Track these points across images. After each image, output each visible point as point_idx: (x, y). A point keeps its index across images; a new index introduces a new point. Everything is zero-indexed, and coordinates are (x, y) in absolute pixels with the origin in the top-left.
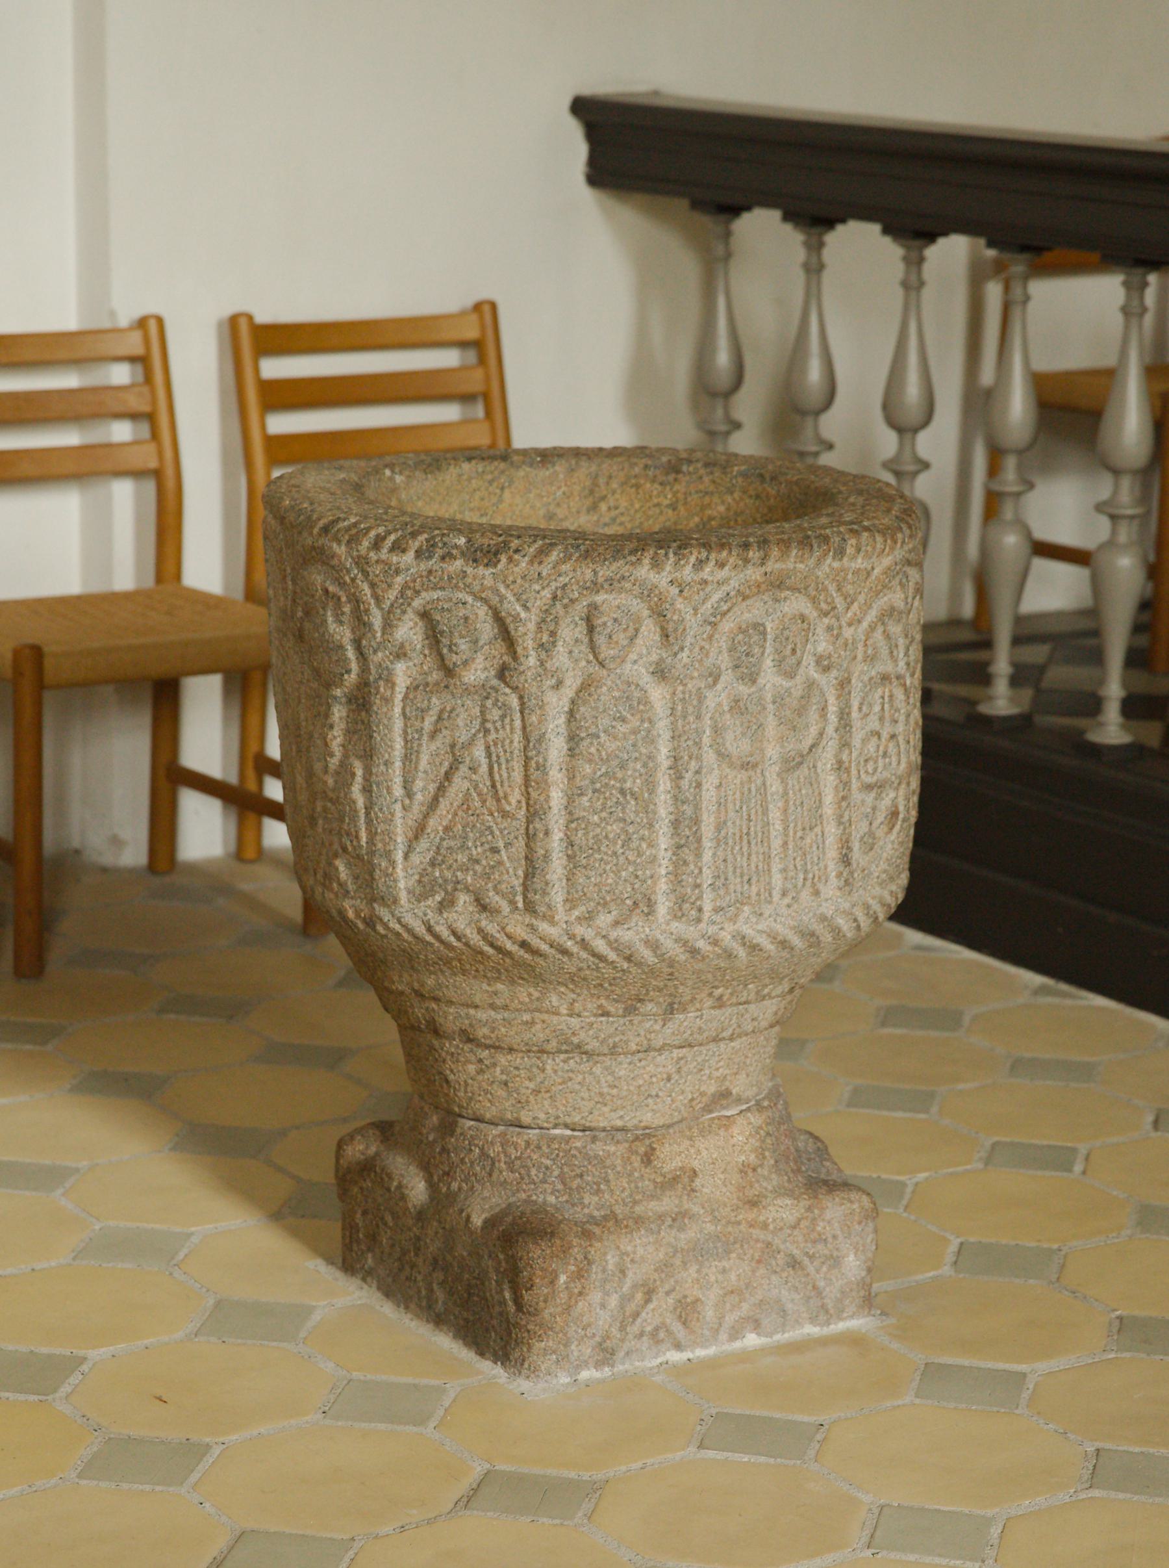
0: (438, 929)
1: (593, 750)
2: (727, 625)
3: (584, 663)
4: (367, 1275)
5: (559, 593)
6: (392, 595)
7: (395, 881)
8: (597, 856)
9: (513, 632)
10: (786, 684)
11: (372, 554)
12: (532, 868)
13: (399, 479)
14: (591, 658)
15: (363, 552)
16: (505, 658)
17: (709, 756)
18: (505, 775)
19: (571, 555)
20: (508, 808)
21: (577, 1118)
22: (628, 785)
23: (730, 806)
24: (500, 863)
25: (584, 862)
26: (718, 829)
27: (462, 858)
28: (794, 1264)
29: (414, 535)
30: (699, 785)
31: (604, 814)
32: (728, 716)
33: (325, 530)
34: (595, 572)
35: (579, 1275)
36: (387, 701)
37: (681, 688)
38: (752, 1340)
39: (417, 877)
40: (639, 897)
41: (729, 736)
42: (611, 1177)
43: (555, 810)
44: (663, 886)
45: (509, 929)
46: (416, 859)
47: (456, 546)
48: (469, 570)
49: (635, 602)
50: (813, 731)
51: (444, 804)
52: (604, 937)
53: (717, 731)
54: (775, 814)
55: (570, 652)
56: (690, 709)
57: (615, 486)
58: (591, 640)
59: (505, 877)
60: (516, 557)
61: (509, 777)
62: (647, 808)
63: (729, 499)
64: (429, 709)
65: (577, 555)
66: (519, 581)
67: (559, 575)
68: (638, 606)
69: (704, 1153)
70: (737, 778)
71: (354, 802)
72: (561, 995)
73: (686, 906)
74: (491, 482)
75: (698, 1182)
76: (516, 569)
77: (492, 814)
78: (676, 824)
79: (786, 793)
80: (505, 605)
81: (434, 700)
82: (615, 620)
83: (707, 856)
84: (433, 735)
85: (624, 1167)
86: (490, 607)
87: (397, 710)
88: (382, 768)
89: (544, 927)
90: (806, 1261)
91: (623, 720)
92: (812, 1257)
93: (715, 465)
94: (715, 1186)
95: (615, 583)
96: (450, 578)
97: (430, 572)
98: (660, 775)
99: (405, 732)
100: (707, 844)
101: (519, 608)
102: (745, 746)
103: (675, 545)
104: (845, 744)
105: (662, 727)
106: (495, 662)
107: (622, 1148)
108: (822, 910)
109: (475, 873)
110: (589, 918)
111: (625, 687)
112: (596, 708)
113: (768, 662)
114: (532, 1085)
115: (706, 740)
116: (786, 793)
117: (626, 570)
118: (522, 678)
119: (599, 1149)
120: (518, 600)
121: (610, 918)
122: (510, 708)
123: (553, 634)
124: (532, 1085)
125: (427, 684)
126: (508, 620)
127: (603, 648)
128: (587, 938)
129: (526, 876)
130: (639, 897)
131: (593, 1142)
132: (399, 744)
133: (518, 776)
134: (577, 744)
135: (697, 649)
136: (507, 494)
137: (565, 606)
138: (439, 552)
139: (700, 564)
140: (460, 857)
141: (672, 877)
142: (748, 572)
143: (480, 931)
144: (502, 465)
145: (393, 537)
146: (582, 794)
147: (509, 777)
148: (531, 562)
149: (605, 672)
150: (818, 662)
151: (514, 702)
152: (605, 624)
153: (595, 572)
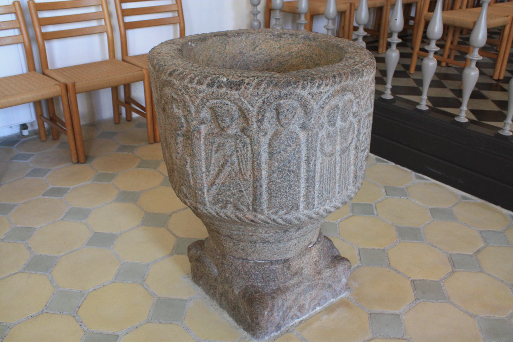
0: (220, 214)
1: (278, 157)
2: (327, 107)
3: (274, 125)
4: (199, 285)
5: (266, 100)
6: (198, 101)
7: (204, 198)
8: (279, 193)
9: (247, 116)
10: (344, 124)
11: (189, 85)
12: (256, 198)
13: (193, 45)
14: (277, 123)
15: (186, 84)
16: (244, 124)
17: (319, 154)
18: (245, 166)
19: (270, 85)
20: (246, 178)
21: (266, 259)
22: (291, 168)
23: (325, 170)
24: (243, 196)
25: (275, 195)
26: (321, 177)
27: (229, 193)
28: (330, 286)
29: (206, 77)
30: (315, 165)
31: (282, 179)
32: (326, 139)
33: (171, 74)
34: (280, 92)
35: (272, 310)
36: (198, 139)
37: (311, 132)
38: (318, 308)
39: (212, 198)
40: (294, 205)
41: (326, 146)
42: (278, 275)
43: (264, 178)
44: (302, 199)
45: (246, 216)
46: (212, 192)
47: (223, 82)
48: (229, 92)
49: (295, 102)
50: (350, 138)
51: (221, 175)
52: (281, 218)
53: (322, 145)
54: (338, 168)
55: (269, 122)
56: (314, 139)
57: (261, 42)
58: (278, 117)
59: (245, 200)
60: (248, 86)
61: (246, 167)
62: (298, 176)
63: (298, 46)
64: (214, 142)
65: (272, 85)
66: (249, 96)
67: (266, 93)
68: (296, 104)
69: (305, 261)
70: (327, 159)
71: (188, 171)
72: (263, 229)
73: (310, 205)
74: (222, 43)
75: (303, 271)
76: (248, 91)
77: (240, 179)
78: (307, 179)
79: (341, 160)
80: (244, 105)
81: (216, 139)
82: (288, 110)
83: (317, 187)
84: (216, 152)
85: (282, 272)
86: (238, 106)
87: (202, 142)
88: (197, 162)
89: (259, 216)
90: (333, 284)
91: (290, 146)
92: (333, 282)
93: (293, 35)
94: (307, 271)
95: (288, 96)
96: (221, 95)
97: (213, 92)
98: (302, 163)
99: (205, 149)
100: (317, 183)
101: (249, 106)
102: (331, 148)
103: (309, 78)
104: (358, 140)
105: (304, 147)
106: (240, 125)
107: (281, 266)
108: (348, 193)
109: (234, 198)
110: (276, 213)
111: (291, 134)
112: (280, 142)
113: (339, 118)
114: (252, 250)
115: (318, 149)
116: (341, 160)
117: (292, 91)
118: (251, 133)
119: (273, 267)
120: (249, 103)
121: (283, 212)
122: (246, 143)
123: (263, 116)
124: (252, 250)
125: (213, 133)
126: (245, 111)
127: (283, 120)
128: (275, 219)
129: (253, 200)
130: (294, 205)
131: (272, 265)
132: (203, 154)
133: (250, 167)
134: (272, 156)
135: (317, 118)
136: (227, 46)
137: (268, 105)
138: (216, 85)
139: (320, 86)
140: (228, 193)
141: (305, 197)
142: (335, 87)
143: (236, 216)
144: (225, 37)
145: (197, 78)
146: (274, 173)
147: (246, 167)
148: (254, 89)
149: (283, 129)
150: (353, 115)
151: (248, 140)
152: (284, 111)
153: (280, 92)
